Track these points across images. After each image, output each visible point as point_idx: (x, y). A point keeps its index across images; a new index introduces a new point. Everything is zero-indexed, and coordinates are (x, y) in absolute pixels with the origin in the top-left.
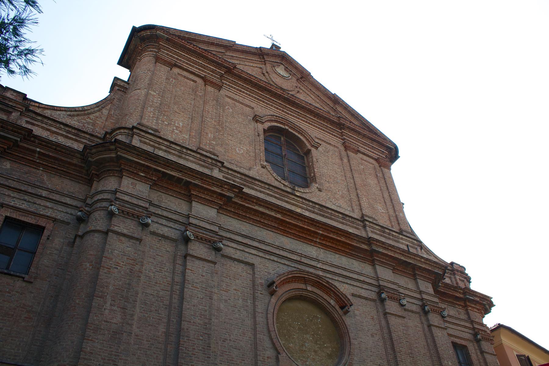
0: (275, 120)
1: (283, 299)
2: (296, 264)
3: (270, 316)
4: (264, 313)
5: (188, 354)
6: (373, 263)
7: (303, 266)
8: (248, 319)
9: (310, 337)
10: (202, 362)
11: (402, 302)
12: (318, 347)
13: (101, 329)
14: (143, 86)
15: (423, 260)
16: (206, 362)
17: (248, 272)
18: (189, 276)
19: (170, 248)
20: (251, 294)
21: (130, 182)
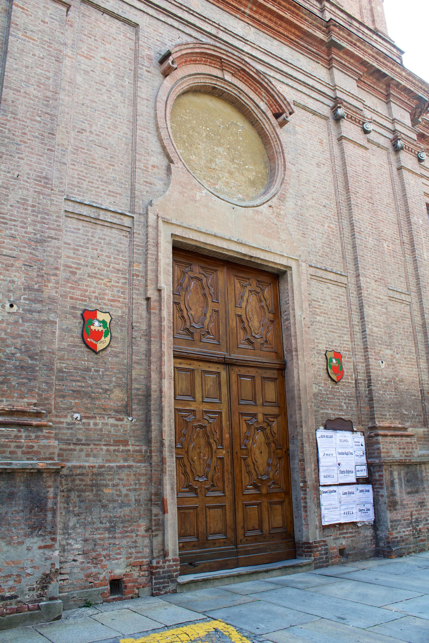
3: (161, 106)
4: (152, 100)
5: (14, 140)
8: (124, 106)
9: (223, 152)
10: (39, 155)
11: (367, 126)
12: (235, 168)
15: (404, 74)
16: (45, 156)
17: (128, 35)
18: (18, 18)
20: (131, 70)
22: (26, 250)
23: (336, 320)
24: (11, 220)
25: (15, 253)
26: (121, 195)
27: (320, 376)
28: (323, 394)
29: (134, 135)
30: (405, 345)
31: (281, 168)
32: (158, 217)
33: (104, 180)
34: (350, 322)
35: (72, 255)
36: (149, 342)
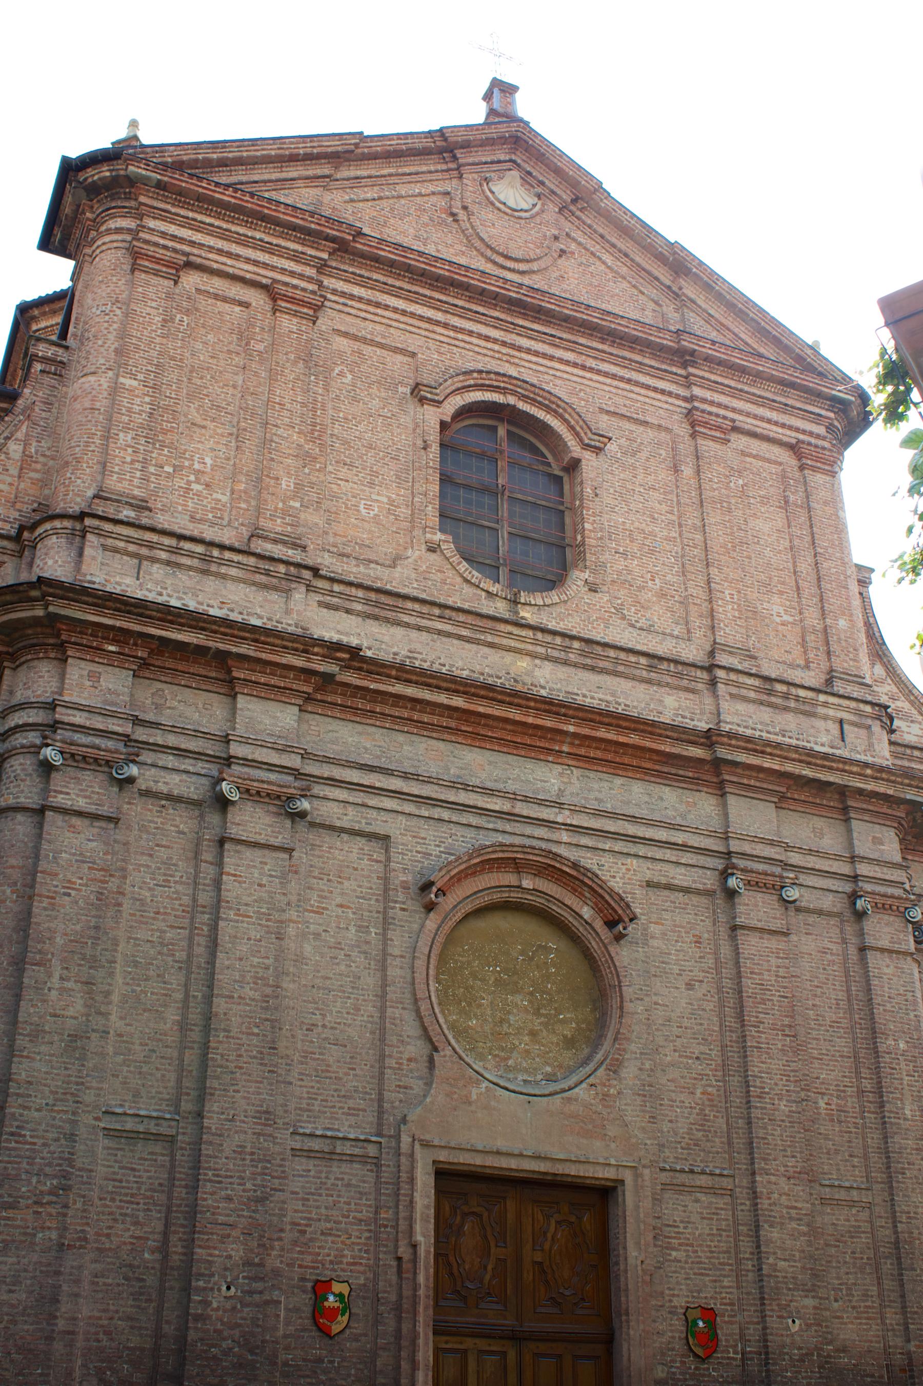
0: (476, 385)
1: (459, 915)
2: (499, 821)
4: (408, 955)
5: (227, 1067)
6: (720, 790)
7: (518, 825)
10: (257, 1082)
12: (541, 1024)
13: (44, 1032)
14: (102, 361)
15: (869, 772)
18: (229, 891)
19: (186, 823)
20: (378, 912)
21: (85, 673)
22: (245, 1213)
23: (708, 1254)
24: (227, 1177)
25: (231, 1220)
26: (365, 1110)
27: (673, 1349)
28: (679, 1380)
29: (383, 1017)
30: (855, 1284)
31: (616, 1013)
32: (414, 1140)
33: (343, 1093)
34: (736, 1253)
35: (301, 1208)
36: (399, 1319)
